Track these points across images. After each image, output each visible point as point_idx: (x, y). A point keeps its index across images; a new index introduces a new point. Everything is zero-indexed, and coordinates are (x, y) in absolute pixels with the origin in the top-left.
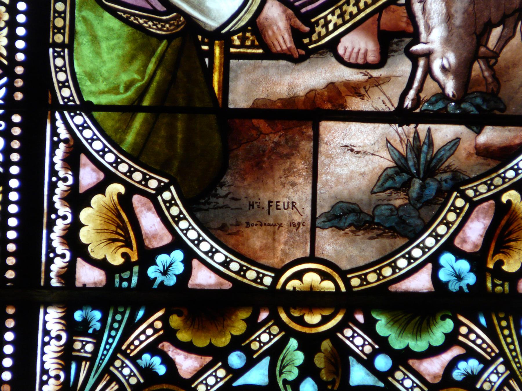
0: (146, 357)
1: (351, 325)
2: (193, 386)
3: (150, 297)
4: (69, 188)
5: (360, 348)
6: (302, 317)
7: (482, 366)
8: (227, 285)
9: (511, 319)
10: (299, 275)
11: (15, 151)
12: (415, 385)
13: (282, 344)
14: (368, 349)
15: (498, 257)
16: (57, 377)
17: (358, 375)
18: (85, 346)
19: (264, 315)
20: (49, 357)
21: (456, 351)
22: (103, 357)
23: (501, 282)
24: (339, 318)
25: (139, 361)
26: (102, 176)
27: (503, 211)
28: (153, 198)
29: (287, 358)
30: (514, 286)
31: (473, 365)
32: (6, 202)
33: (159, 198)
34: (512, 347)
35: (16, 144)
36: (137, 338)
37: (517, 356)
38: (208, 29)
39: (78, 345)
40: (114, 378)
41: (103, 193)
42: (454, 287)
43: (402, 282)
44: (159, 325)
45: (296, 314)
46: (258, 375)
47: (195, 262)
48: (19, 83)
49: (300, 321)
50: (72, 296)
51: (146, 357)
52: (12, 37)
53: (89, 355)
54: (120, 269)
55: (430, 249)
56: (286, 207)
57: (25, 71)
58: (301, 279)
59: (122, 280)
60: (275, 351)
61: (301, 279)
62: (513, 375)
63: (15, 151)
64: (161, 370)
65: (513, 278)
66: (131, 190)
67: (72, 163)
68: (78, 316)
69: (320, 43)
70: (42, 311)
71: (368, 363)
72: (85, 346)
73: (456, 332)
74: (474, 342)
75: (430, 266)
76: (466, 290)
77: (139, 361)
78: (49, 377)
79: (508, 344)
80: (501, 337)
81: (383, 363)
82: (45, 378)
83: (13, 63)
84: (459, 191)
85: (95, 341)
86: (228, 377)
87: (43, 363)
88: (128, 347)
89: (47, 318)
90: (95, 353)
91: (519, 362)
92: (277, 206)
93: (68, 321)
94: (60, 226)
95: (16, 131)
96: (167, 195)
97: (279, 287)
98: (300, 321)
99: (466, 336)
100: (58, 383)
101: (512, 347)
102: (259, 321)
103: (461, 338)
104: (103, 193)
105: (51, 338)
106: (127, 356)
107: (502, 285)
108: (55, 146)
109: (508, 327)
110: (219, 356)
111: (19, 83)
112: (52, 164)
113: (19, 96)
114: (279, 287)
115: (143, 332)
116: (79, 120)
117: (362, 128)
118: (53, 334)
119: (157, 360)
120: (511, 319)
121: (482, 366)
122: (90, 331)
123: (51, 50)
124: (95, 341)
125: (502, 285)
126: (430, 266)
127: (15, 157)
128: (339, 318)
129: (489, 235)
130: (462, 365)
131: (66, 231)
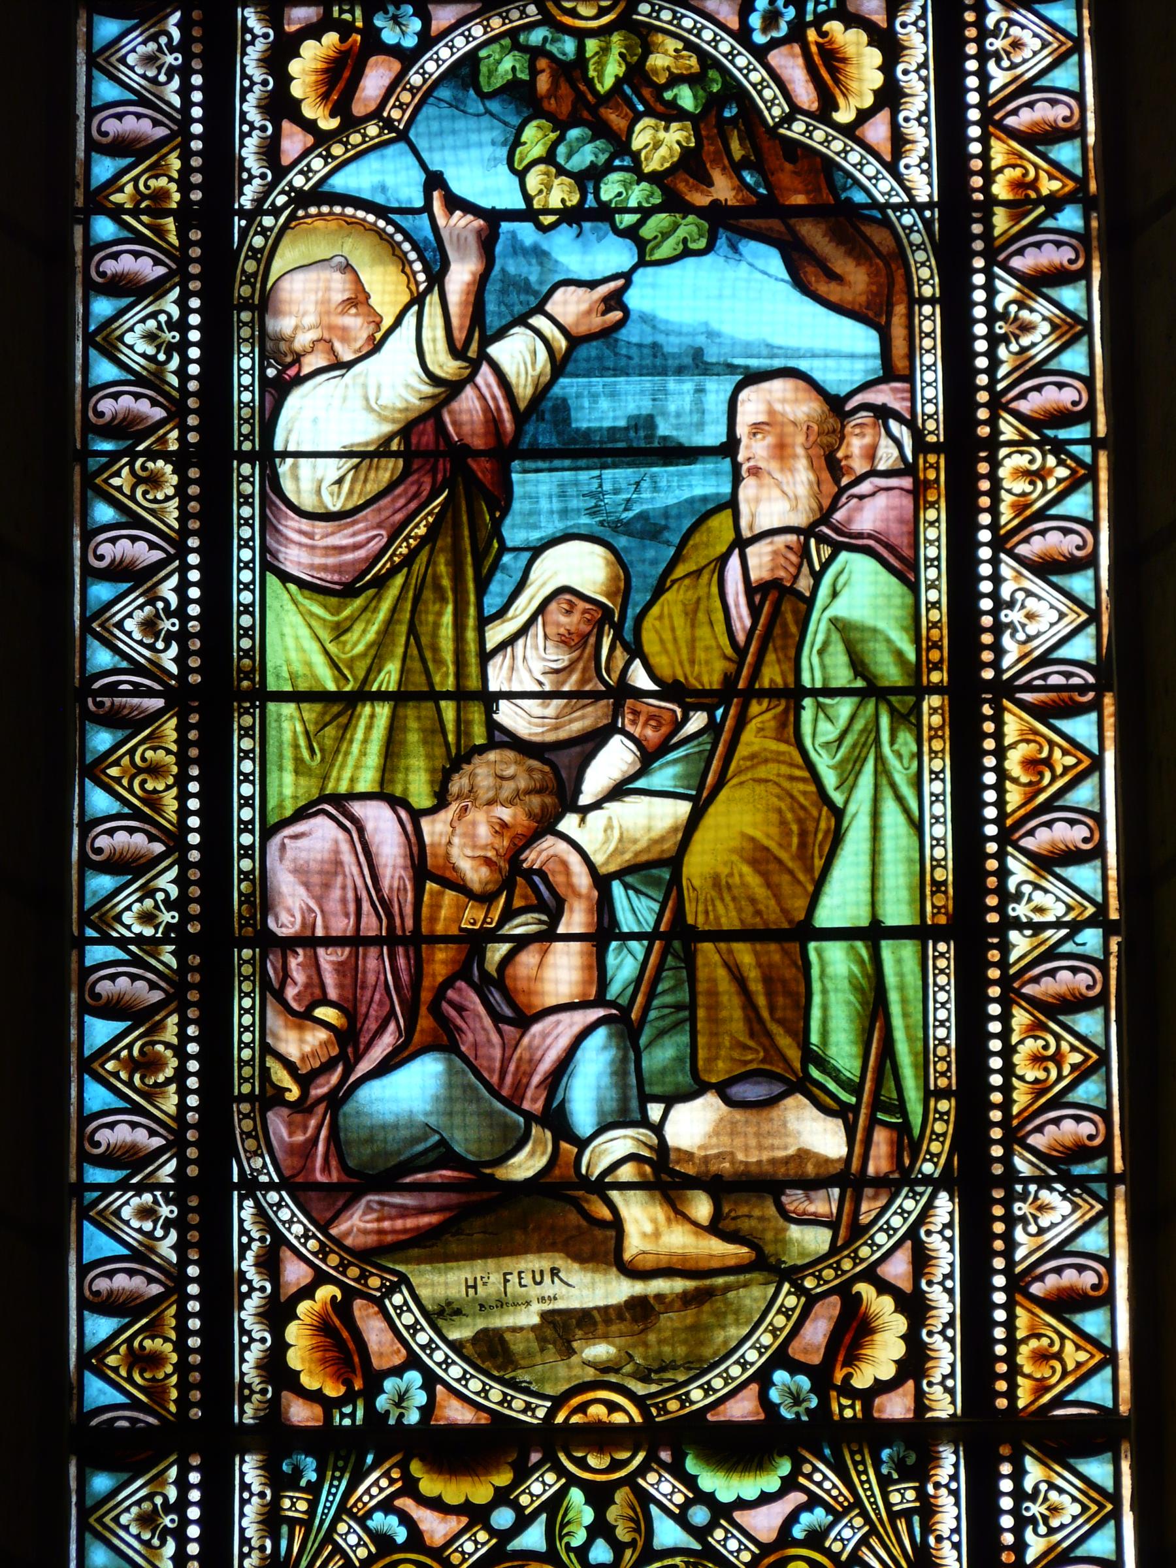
0: (378, 1516)
3: (384, 1440)
8: (484, 1419)
10: (582, 1408)
13: (562, 1493)
14: (679, 1499)
17: (668, 1534)
18: (295, 1505)
19: (535, 1457)
20: (248, 1520)
24: (640, 1457)
25: (370, 1523)
28: (379, 1303)
29: (570, 1515)
30: (868, 1408)
31: (818, 1517)
39: (287, 1503)
40: (338, 1549)
41: (312, 1298)
43: (626, 1244)
44: (395, 1474)
46: (533, 1538)
49: (582, 1464)
50: (275, 1440)
51: (378, 1516)
54: (339, 1402)
59: (343, 1416)
60: (554, 1505)
62: (873, 1531)
64: (401, 1535)
66: (350, 1294)
67: (899, 141)
72: (295, 1505)
73: (796, 1471)
74: (819, 1485)
77: (370, 1523)
79: (859, 1474)
81: (700, 1515)
82: (246, 1495)
89: (245, 1468)
93: (271, 1470)
96: (397, 1299)
97: (560, 1419)
98: (582, 1464)
99: (809, 1477)
103: (802, 1480)
104: (312, 1298)
106: (353, 1516)
107: (852, 1407)
110: (176, 1145)
116: (273, 1197)
119: (393, 1520)
122: (303, 1483)
125: (852, 1407)
126: (754, 1388)
128: (640, 1457)
130: (806, 1519)
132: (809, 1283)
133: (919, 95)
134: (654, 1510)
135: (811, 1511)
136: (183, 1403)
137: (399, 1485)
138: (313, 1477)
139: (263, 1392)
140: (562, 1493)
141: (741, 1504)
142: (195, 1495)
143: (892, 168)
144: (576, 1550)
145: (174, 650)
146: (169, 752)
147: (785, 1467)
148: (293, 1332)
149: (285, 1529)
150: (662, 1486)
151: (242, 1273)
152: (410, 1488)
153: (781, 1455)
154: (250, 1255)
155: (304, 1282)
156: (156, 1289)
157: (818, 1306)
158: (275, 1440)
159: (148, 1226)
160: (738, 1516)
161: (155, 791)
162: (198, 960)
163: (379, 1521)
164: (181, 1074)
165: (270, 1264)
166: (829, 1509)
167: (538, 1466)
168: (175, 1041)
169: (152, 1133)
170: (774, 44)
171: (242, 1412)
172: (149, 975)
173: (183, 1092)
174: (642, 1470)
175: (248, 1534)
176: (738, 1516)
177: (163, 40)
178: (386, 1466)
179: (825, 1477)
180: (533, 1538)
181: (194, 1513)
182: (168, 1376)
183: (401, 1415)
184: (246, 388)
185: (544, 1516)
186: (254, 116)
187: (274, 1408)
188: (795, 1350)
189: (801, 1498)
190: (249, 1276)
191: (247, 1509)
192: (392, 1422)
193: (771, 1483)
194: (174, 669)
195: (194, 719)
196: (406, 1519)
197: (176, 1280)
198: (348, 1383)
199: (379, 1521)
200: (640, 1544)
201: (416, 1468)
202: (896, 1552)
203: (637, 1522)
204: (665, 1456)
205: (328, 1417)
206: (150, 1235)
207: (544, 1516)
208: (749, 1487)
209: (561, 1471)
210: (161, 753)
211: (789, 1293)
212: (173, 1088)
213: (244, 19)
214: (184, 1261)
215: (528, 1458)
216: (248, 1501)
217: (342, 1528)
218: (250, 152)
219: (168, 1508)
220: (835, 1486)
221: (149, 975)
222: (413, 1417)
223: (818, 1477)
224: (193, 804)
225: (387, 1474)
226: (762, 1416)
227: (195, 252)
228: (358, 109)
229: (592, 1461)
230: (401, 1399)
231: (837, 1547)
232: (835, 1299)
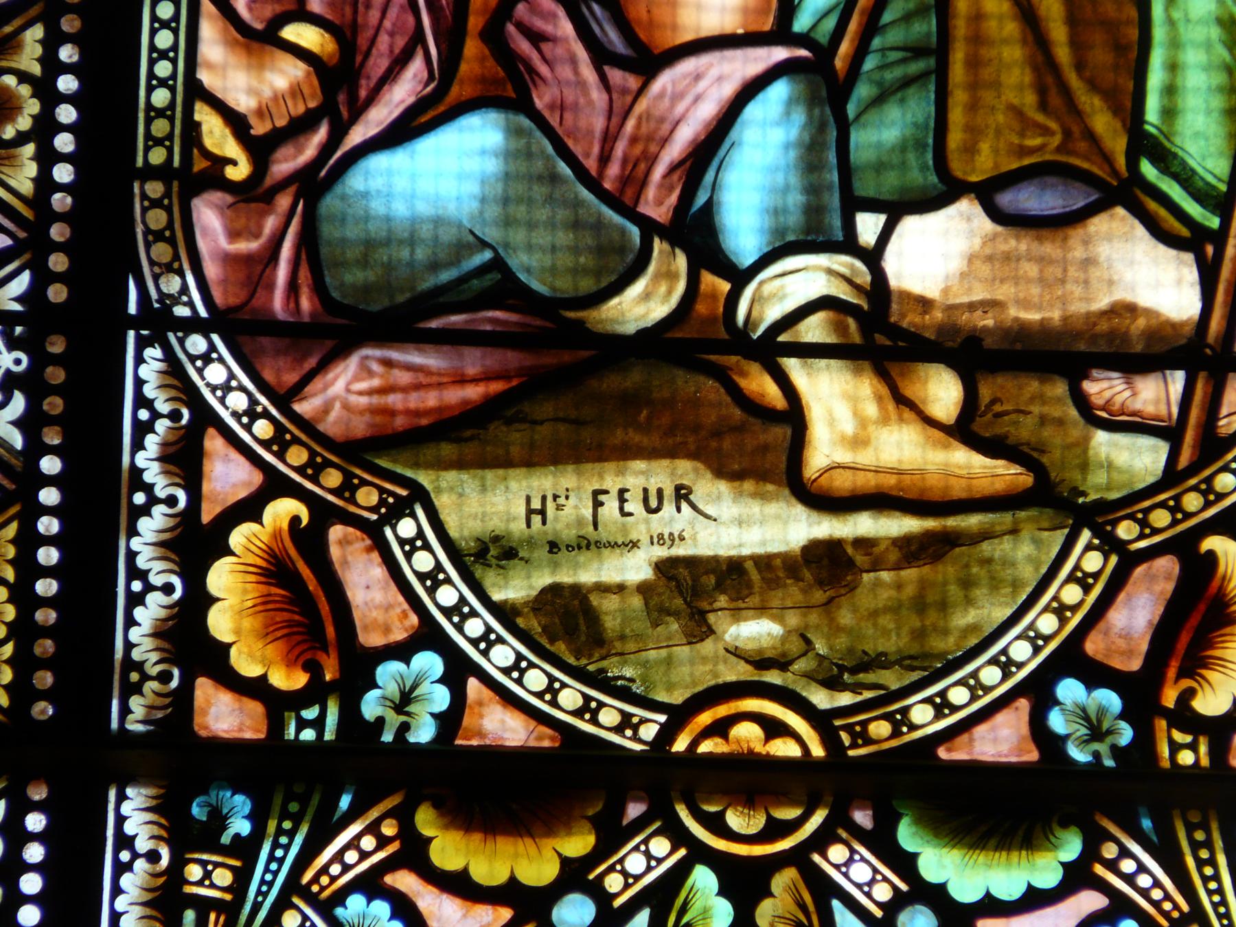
0: (356, 902)
4: (178, 519)
5: (857, 857)
6: (721, 815)
8: (546, 739)
9: (1214, 826)
10: (720, 728)
11: (34, 837)
13: (680, 873)
15: (1186, 683)
16: (153, 857)
19: (634, 810)
20: (127, 902)
22: (260, 899)
23: (1188, 739)
25: (339, 911)
26: (257, 478)
27: (1198, 581)
28: (374, 534)
30: (1219, 752)
32: (15, 866)
33: (388, 532)
34: (1208, 871)
35: (67, 114)
36: (339, 857)
37: (1224, 902)
41: (258, 519)
42: (1079, 755)
44: (389, 829)
47: (473, 684)
48: (48, 525)
50: (182, 764)
51: (356, 902)
52: (23, 663)
54: (297, 700)
55: (1020, 666)
57: (77, 173)
58: (725, 736)
59: (302, 724)
61: (771, 820)
63: (47, 572)
65: (1219, 730)
66: (323, 514)
67: (185, 459)
68: (198, 811)
69: (811, 908)
70: (112, 795)
72: (208, 877)
73: (1090, 853)
75: (1023, 704)
76: (1109, 763)
77: (339, 911)
78: (135, 856)
79: (1210, 893)
80: (1184, 844)
82: (125, 856)
83: (46, 215)
87: (121, 819)
88: (316, 879)
89: (126, 808)
91: (1227, 915)
96: (406, 528)
97: (680, 745)
98: (717, 825)
99: (1112, 866)
100: (166, 600)
101: (1208, 871)
102: (625, 822)
103: (1099, 869)
104: (258, 519)
106: (312, 900)
107: (1193, 746)
108: (142, 430)
112: (139, 383)
113: (57, 293)
115: (353, 844)
120: (1214, 826)
122: (226, 839)
123: (131, 334)
129: (1164, 634)
132: (1126, 530)
138: (240, 826)
140: (680, 873)
142: (34, 853)
143: (205, 418)
148: (221, 577)
151: (136, 472)
152: (413, 854)
153: (1065, 825)
154: (152, 442)
157: (1140, 571)
164: (45, 127)
165: (185, 459)
167: (639, 825)
168: (36, 69)
171: (125, 711)
173: (47, 158)
174: (821, 840)
178: (374, 814)
179: (1142, 868)
183: (404, 728)
184: (165, 25)
186: (152, 473)
187: (181, 704)
188: (1093, 646)
190: (148, 477)
192: (388, 737)
198: (313, 668)
201: (425, 821)
204: (863, 818)
209: (679, 836)
211: (1089, 547)
212: (29, 149)
214: (35, 448)
215: (622, 812)
218: (140, 630)
220: (1157, 884)
222: (424, 733)
225: (373, 829)
228: (1167, 565)
229: (734, 820)
230: (405, 700)
232: (1167, 565)
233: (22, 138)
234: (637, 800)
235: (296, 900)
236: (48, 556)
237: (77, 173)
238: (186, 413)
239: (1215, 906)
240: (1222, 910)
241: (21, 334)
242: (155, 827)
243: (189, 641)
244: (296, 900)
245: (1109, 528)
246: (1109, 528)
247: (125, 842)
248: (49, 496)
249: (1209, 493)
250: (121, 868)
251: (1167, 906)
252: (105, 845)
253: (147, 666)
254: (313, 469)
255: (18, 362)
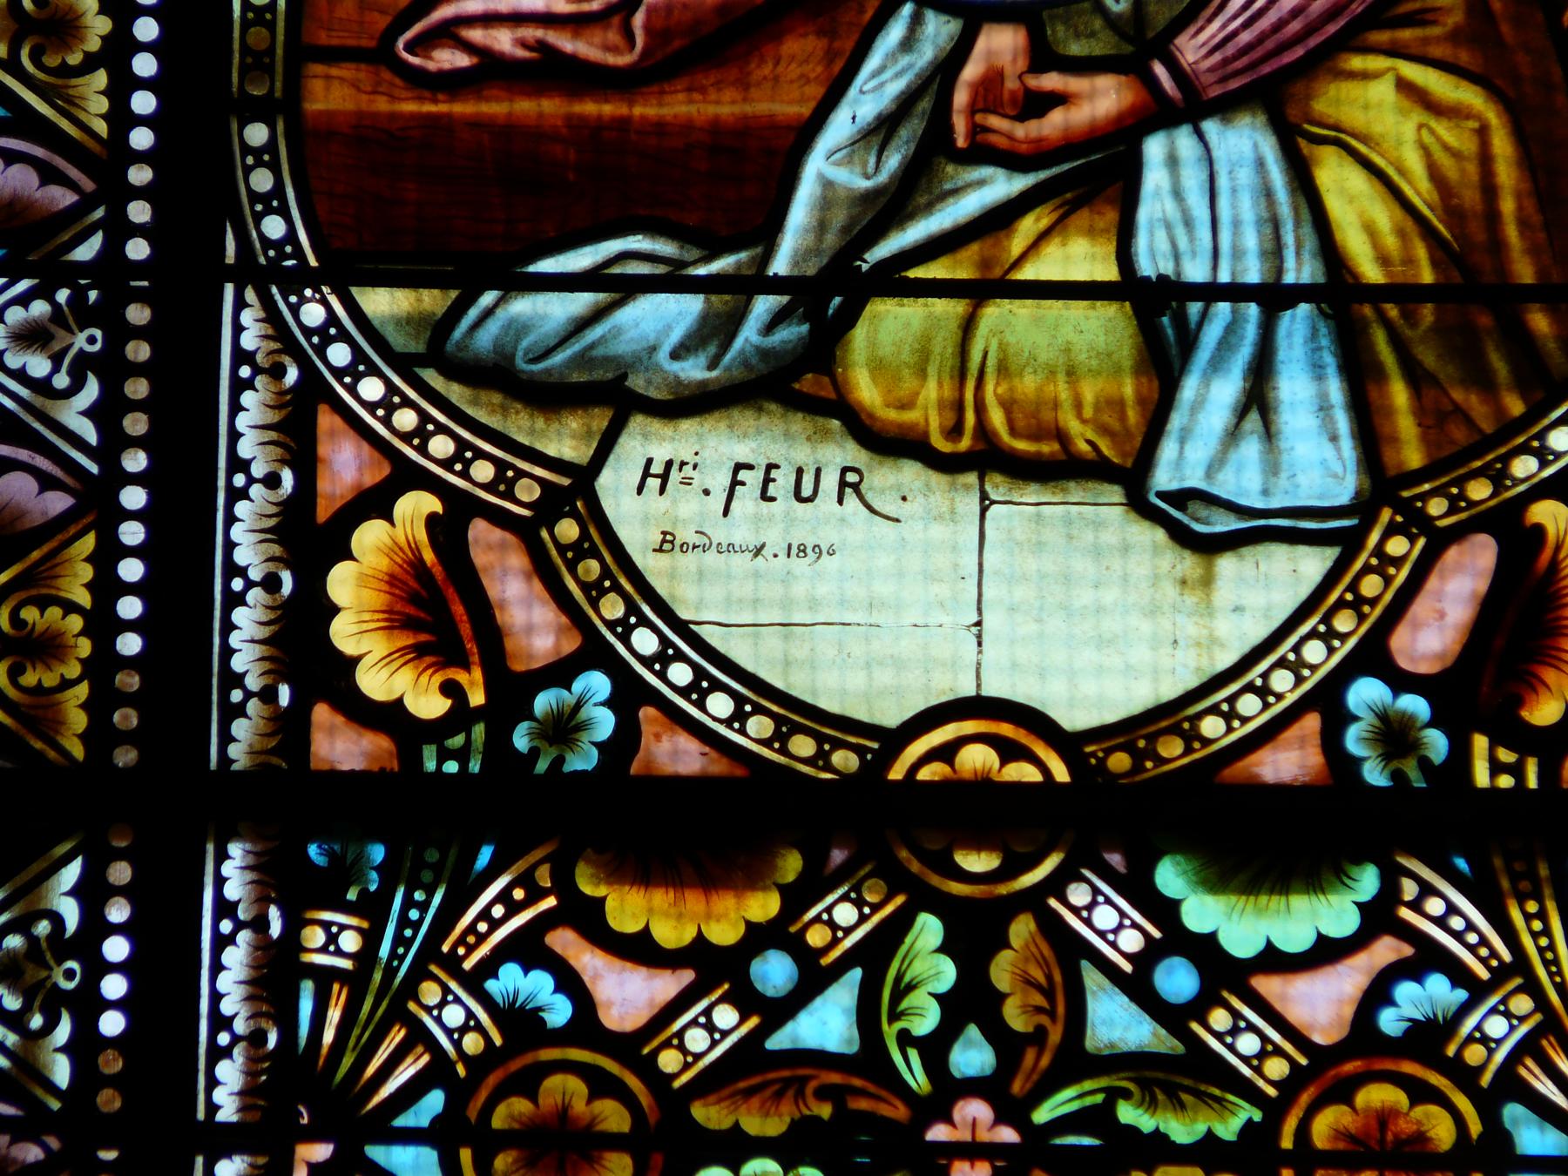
1: (1087, 873)
2: (646, 1051)
7: (1461, 995)
12: (1270, 1048)
19: (838, 856)
21: (1387, 950)
25: (491, 985)
27: (1525, 569)
37: (1552, 947)
38: (796, 976)
44: (544, 878)
45: (934, 846)
46: (827, 1024)
47: (647, 714)
50: (292, 811)
53: (346, 964)
56: (807, 491)
58: (950, 761)
61: (950, 761)
64: (559, 1012)
67: (296, 435)
71: (1137, 985)
72: (331, 939)
73: (1389, 894)
74: (1440, 922)
77: (491, 985)
78: (251, 480)
79: (1535, 936)
81: (1177, 980)
82: (239, 480)
84: (1401, 506)
85: (365, 925)
86: (744, 1030)
89: (228, 869)
90: (365, 957)
92: (768, 480)
94: (248, 620)
95: (139, 351)
97: (897, 773)
99: (1416, 906)
103: (1405, 913)
105: (249, 695)
109: (1542, 915)
111: (138, 388)
114: (897, 773)
117: (1205, 662)
118: (258, 470)
121: (1461, 995)
124: (365, 925)
126: (1311, 723)
127: (131, 570)
130: (1405, 991)
131: (284, 412)
133: (246, 540)
134: (1092, 977)
135: (1419, 978)
136: (100, 735)
137: (551, 902)
139: (277, 372)
141: (1273, 960)
142: (114, 986)
144: (922, 1043)
145: (91, 391)
146: (70, 607)
147: (1368, 882)
149: (307, 989)
150: (1109, 922)
155: (370, 479)
156: (64, 198)
158: (292, 811)
159: (39, 366)
160: (1268, 986)
161: (39, 689)
162: (119, 1065)
163: (510, 981)
164: (120, 47)
166: (1458, 974)
169: (47, 483)
170: (561, 672)
171: (226, 738)
172: (42, 462)
173: (123, 85)
174: (1056, 884)
175: (227, 1007)
176: (1268, 986)
177: (43, 928)
180: (827, 1024)
181: (116, 949)
182: (66, 684)
185: (856, 974)
187: (290, 731)
189: (1387, 950)
191: (240, 615)
193: (1336, 913)
194: (90, 434)
195: (121, 873)
196: (569, 982)
197: (96, 504)
199: (510, 981)
200: (1055, 1036)
202: (347, 1061)
203: (1048, 993)
204: (1115, 860)
205: (410, 757)
206: (42, 387)
207: (856, 974)
208: (1298, 920)
210: (54, 612)
212: (101, 79)
213: (238, 329)
215: (826, 857)
216: (230, 940)
217: (430, 993)
218: (246, 633)
219: (61, 945)
220: (1470, 926)
221: (42, 462)
223: (1435, 906)
224: (131, 570)
226: (1331, 782)
227: (130, 607)
230: (564, 728)
231: (1475, 1054)
233: (90, 63)
234: (840, 847)
235: (434, 969)
236: (130, 607)
237: (152, 423)
238: (287, 578)
239: (1541, 950)
240: (1549, 956)
241: (96, 301)
242: (272, 447)
243: (302, 632)
244: (434, 969)
245: (1419, 504)
246: (1419, 504)
247: (238, 464)
248: (139, 212)
249: (1544, 455)
250: (236, 495)
251: (1484, 952)
252: (200, 968)
253: (259, 358)
254: (462, 457)
255: (92, 340)
